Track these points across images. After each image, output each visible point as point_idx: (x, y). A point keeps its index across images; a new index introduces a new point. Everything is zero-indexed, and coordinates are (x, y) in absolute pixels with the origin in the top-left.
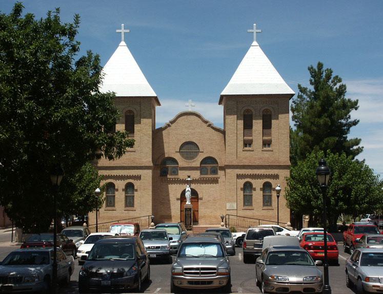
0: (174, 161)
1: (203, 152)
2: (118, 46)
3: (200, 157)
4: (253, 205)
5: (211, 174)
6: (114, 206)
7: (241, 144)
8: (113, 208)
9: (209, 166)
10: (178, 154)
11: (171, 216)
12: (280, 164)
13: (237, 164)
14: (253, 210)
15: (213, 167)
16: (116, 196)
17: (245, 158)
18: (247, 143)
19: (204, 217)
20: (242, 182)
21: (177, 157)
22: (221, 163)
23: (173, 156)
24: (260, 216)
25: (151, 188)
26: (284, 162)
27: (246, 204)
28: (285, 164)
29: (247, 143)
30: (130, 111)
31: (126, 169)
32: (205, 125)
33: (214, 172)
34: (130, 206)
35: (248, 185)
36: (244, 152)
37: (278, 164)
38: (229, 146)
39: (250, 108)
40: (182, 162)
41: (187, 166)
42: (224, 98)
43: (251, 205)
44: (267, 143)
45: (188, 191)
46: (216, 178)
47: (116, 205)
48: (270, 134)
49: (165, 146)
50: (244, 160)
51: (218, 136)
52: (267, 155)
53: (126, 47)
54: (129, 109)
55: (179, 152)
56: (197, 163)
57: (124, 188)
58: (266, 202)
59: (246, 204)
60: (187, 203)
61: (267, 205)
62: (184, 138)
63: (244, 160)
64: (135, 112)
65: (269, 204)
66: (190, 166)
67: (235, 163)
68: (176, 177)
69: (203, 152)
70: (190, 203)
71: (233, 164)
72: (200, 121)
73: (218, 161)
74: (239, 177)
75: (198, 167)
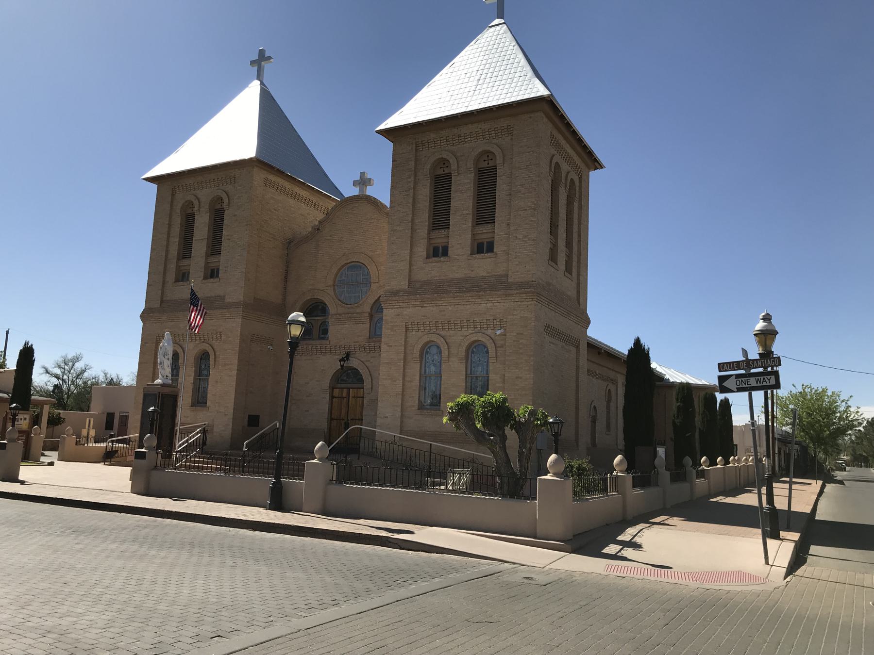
7: (421, 250)
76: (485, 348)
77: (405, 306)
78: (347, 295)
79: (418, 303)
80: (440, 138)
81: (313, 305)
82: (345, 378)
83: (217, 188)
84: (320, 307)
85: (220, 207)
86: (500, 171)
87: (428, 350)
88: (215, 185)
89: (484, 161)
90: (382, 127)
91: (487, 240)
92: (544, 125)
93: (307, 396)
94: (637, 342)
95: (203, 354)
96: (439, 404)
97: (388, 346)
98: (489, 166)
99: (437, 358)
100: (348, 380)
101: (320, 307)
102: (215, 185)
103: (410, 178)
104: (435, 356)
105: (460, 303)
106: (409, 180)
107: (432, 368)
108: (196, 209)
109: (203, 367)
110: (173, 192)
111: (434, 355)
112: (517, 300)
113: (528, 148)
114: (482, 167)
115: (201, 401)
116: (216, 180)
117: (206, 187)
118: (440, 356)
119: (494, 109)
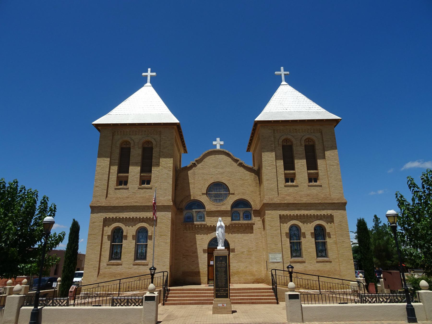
0: (200, 205)
1: (233, 194)
2: (143, 86)
3: (231, 200)
4: (304, 256)
5: (244, 219)
6: (120, 259)
7: (282, 178)
8: (119, 261)
9: (241, 210)
10: (205, 196)
11: (199, 272)
12: (333, 202)
13: (279, 202)
14: (304, 262)
15: (246, 211)
16: (123, 245)
17: (289, 195)
18: (290, 179)
19: (238, 273)
20: (286, 227)
21: (204, 199)
22: (256, 204)
23: (198, 198)
24: (314, 271)
25: (169, 234)
26: (338, 199)
27: (294, 254)
28: (339, 201)
29: (290, 179)
30: (149, 142)
31: (265, 304)
32: (235, 165)
33: (248, 216)
34: (141, 259)
35: (294, 229)
36: (286, 188)
37: (330, 202)
38: (268, 180)
39: (289, 137)
40: (210, 206)
41: (215, 209)
42: (259, 125)
43: (300, 256)
44: (313, 178)
45: (221, 227)
46: (250, 224)
47: (122, 257)
48: (316, 168)
49: (191, 186)
50: (288, 198)
51: (249, 177)
52: (315, 191)
53: (152, 88)
54: (149, 139)
55: (206, 194)
56: (227, 205)
57: (135, 234)
58: (320, 252)
59: (294, 254)
60: (219, 248)
61: (322, 256)
62: (212, 177)
63: (288, 198)
64: (154, 143)
65: (324, 254)
66: (219, 209)
67: (277, 200)
68: (203, 223)
69: (233, 194)
70: (223, 248)
71: (273, 202)
72: (229, 160)
73: (252, 203)
74: (283, 219)
75: (228, 211)
76: (321, 228)
77: (278, 206)
78: (214, 198)
79: (286, 205)
80: (130, 131)
81: (192, 203)
82: (214, 243)
83: (147, 136)
84: (196, 204)
85: (286, 144)
86: (154, 150)
87: (291, 228)
88: (145, 134)
89: (307, 142)
90: (96, 122)
91: (314, 177)
92: (175, 133)
93: (192, 253)
94: (74, 220)
95: (140, 230)
96: (300, 256)
97: (270, 226)
98: (309, 144)
99: (296, 232)
100: (216, 244)
101: (196, 204)
102: (145, 134)
103: (272, 145)
104: (295, 231)
105: (308, 206)
106: (272, 146)
107: (294, 238)
108: (131, 145)
109: (141, 237)
110: (113, 134)
111: (294, 231)
112: (337, 206)
113: (330, 139)
114: (146, 147)
115: (139, 258)
116: (147, 131)
117: (139, 134)
118: (298, 231)
119: (162, 124)
